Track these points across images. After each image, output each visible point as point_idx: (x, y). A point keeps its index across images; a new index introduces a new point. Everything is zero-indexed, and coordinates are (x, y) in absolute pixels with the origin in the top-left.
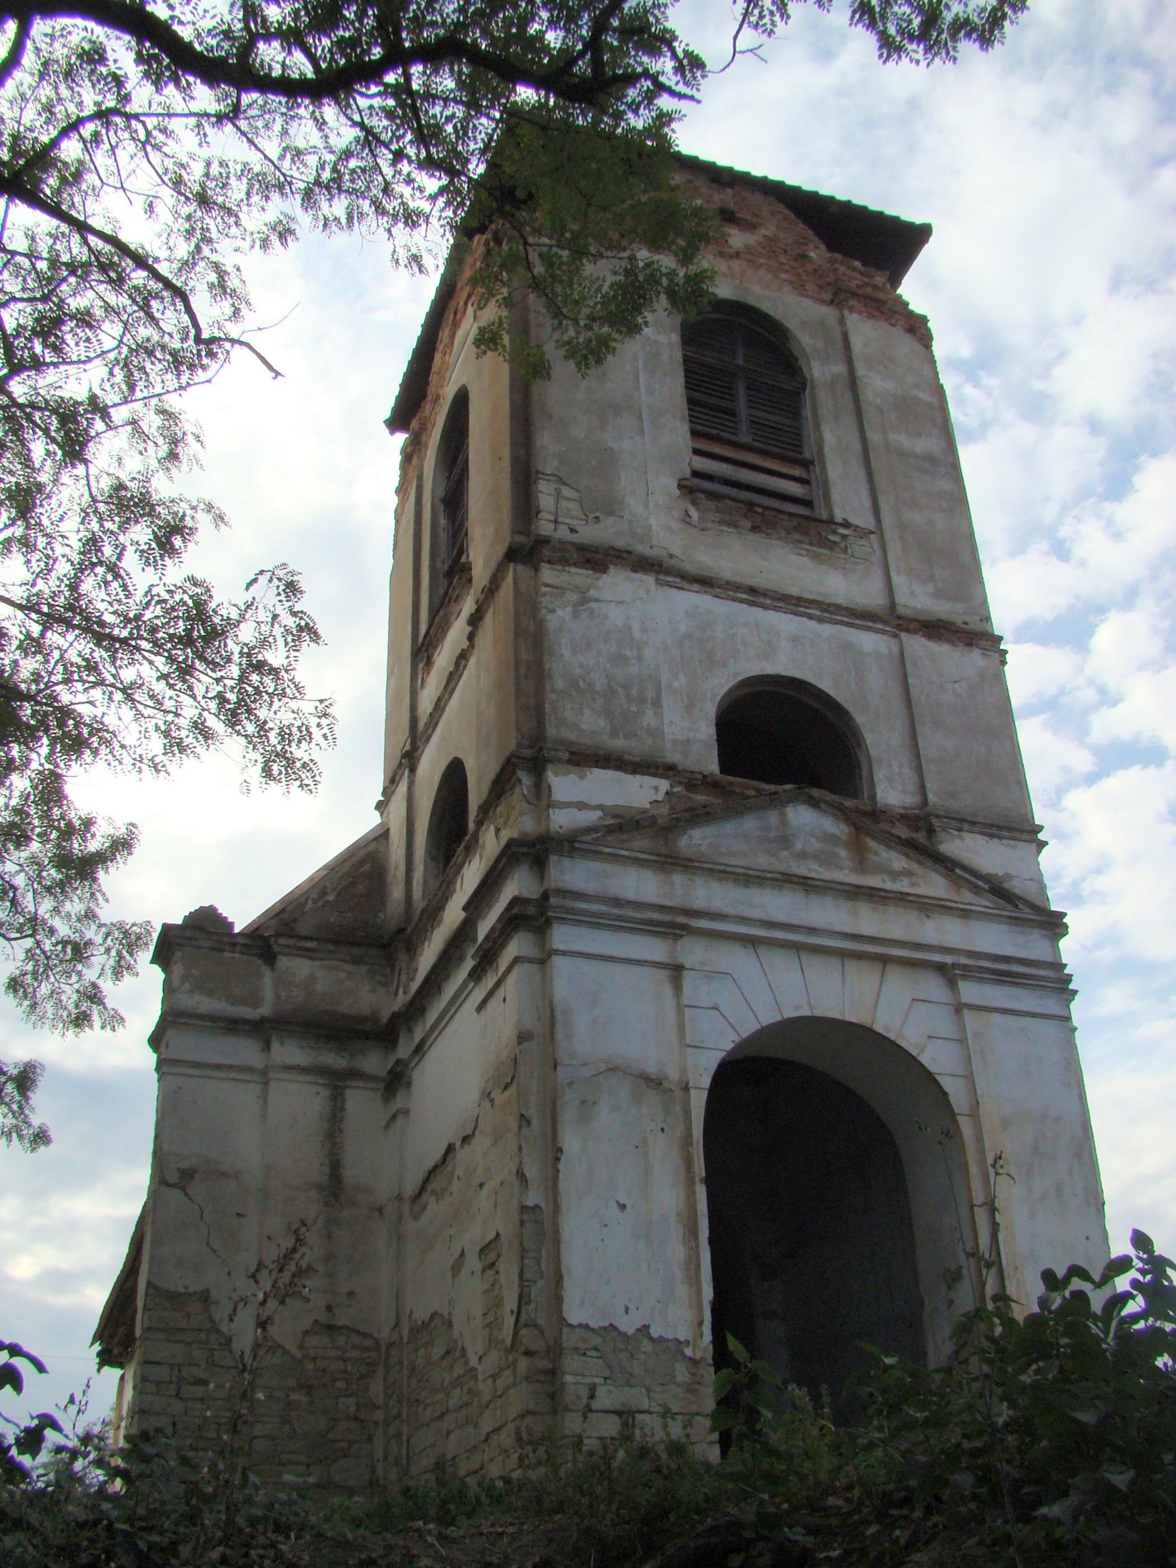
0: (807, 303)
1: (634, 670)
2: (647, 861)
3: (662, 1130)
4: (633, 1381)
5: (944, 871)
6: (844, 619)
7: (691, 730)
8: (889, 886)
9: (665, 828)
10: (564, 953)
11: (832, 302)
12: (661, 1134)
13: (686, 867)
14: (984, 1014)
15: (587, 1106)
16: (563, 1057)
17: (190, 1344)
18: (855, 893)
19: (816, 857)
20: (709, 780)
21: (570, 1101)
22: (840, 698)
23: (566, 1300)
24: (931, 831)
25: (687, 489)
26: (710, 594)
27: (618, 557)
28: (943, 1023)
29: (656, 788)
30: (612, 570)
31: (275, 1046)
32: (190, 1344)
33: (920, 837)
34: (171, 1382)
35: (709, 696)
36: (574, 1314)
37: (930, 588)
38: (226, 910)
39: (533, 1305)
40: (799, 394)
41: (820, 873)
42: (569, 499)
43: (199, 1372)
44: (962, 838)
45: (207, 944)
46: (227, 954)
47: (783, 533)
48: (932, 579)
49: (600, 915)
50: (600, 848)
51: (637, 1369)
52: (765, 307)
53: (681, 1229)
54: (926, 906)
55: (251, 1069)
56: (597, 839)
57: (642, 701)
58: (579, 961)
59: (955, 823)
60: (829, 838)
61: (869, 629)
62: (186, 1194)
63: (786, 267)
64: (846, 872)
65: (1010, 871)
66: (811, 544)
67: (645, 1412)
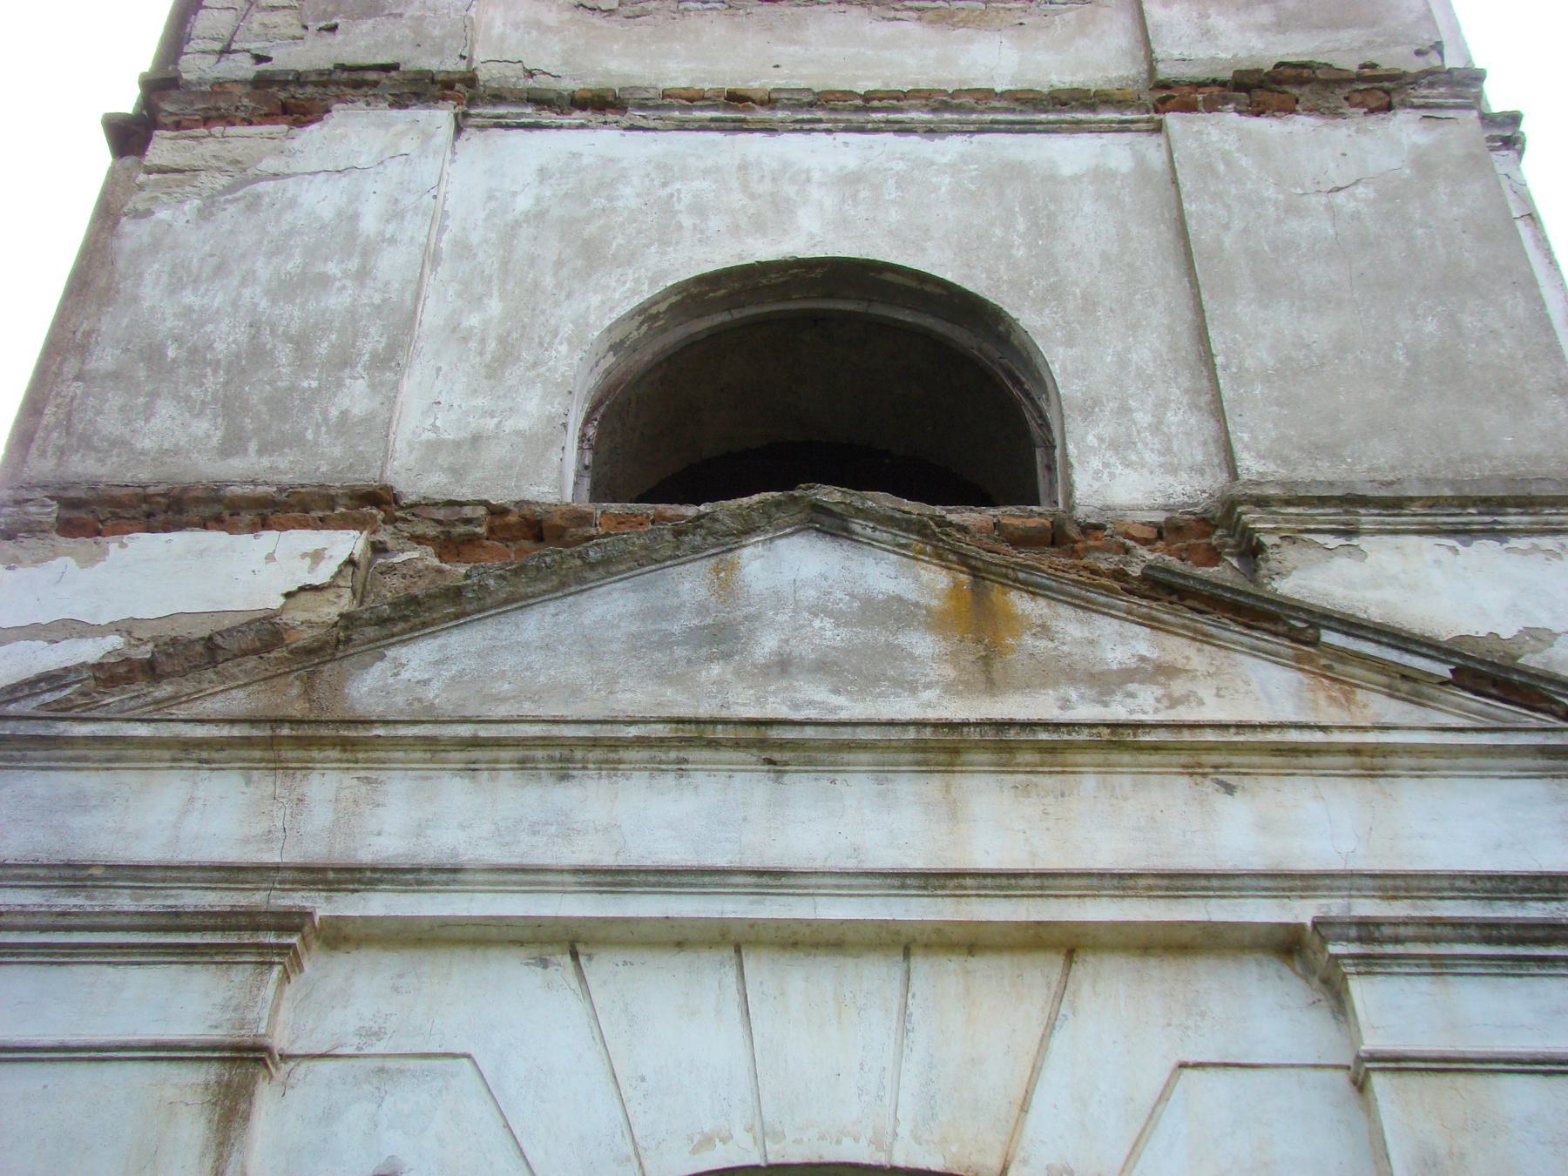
1: (337, 301)
2: (228, 743)
5: (1284, 646)
8: (1085, 712)
9: (309, 651)
13: (346, 744)
19: (824, 667)
20: (512, 519)
22: (975, 282)
24: (1252, 551)
27: (357, 85)
29: (317, 556)
33: (1225, 572)
57: (343, 360)
60: (895, 612)
64: (927, 695)
65: (1543, 620)
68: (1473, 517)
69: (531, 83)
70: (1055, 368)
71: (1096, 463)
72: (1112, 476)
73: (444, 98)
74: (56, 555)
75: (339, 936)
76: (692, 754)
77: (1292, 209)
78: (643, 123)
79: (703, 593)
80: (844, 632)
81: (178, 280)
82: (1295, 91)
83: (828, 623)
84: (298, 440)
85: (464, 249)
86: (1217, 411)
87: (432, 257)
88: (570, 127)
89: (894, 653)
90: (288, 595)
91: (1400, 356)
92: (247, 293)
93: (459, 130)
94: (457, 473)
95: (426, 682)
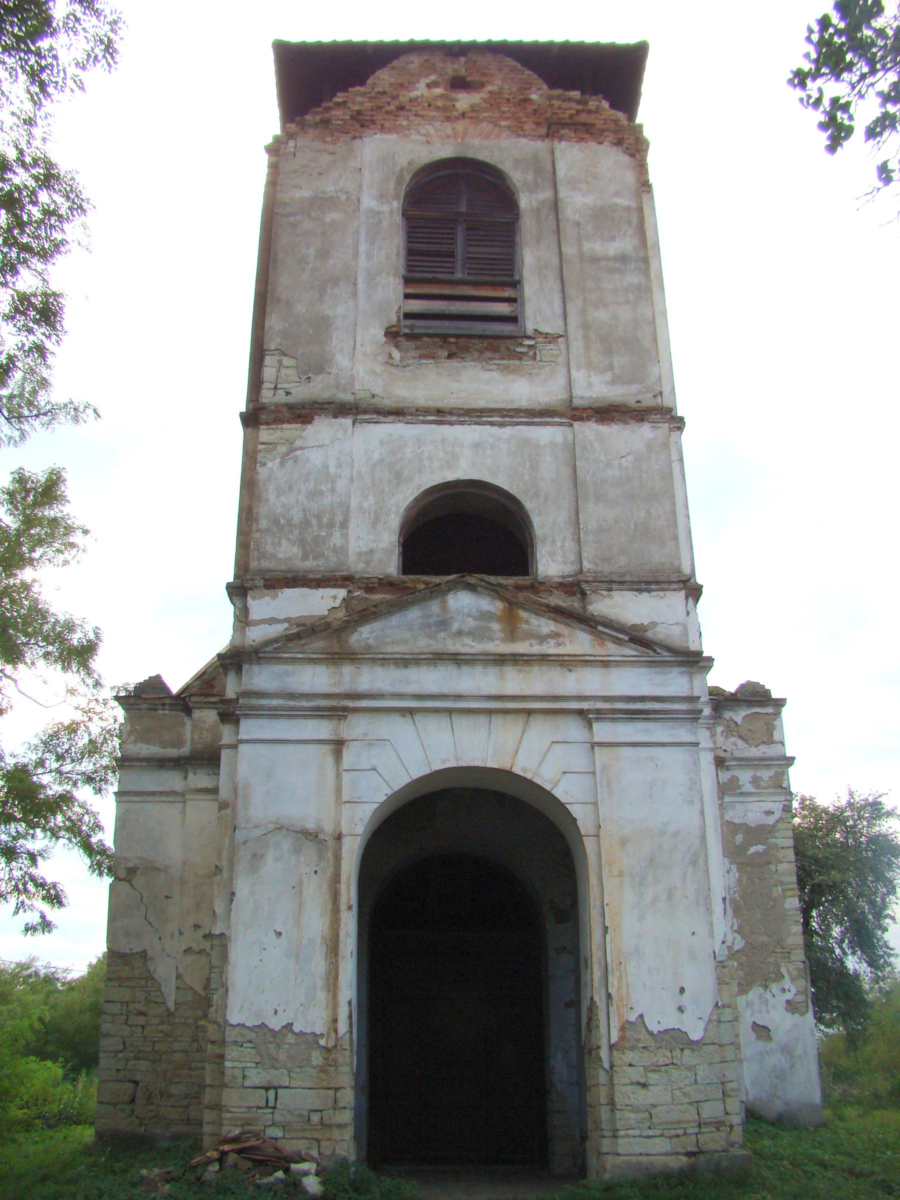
0: (523, 141)
1: (327, 500)
3: (316, 872)
4: (278, 1065)
7: (374, 541)
10: (247, 741)
11: (548, 135)
13: (352, 659)
15: (257, 857)
16: (241, 823)
17: (135, 988)
18: (500, 660)
19: (471, 634)
20: (385, 582)
21: (244, 854)
25: (392, 334)
26: (403, 422)
27: (321, 409)
28: (577, 758)
29: (335, 597)
30: (317, 420)
31: (191, 776)
32: (135, 988)
35: (393, 510)
36: (234, 1017)
37: (608, 376)
39: (214, 1007)
40: (514, 223)
42: (288, 367)
43: (141, 1007)
44: (611, 597)
45: (145, 706)
46: (160, 712)
47: (476, 355)
48: (611, 367)
49: (276, 708)
50: (280, 655)
51: (282, 1056)
52: (482, 156)
54: (568, 663)
55: (174, 793)
57: (331, 525)
58: (259, 746)
59: (604, 585)
60: (485, 616)
61: (546, 424)
62: (132, 885)
64: (497, 642)
65: (656, 619)
66: (502, 359)
68: (643, 586)
69: (373, 401)
70: (535, 525)
71: (544, 561)
73: (349, 414)
75: (355, 710)
77: (609, 465)
79: (438, 610)
80: (475, 623)
81: (279, 493)
82: (614, 414)
83: (471, 619)
84: (322, 555)
86: (579, 542)
89: (489, 629)
91: (632, 525)
92: (300, 497)
93: (354, 424)
94: (367, 563)
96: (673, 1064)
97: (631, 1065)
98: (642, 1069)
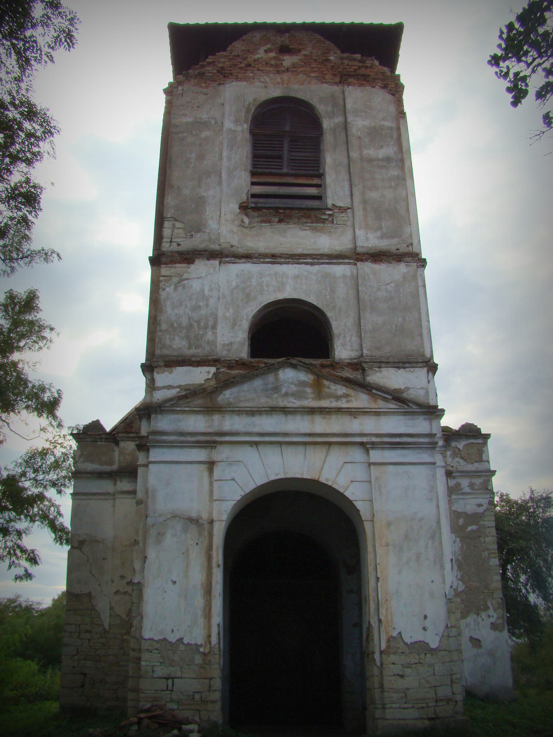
1: (203, 312)
2: (200, 411)
6: (327, 261)
7: (233, 337)
10: (154, 462)
11: (340, 82)
12: (197, 547)
14: (383, 466)
15: (161, 535)
18: (312, 411)
19: (294, 395)
21: (153, 532)
22: (320, 306)
23: (143, 628)
25: (244, 208)
27: (200, 254)
28: (359, 472)
29: (208, 372)
34: (76, 632)
35: (245, 317)
36: (147, 635)
37: (379, 234)
38: (103, 423)
41: (294, 403)
42: (179, 228)
44: (381, 372)
45: (89, 440)
46: (99, 443)
47: (296, 220)
48: (380, 228)
50: (175, 408)
52: (300, 96)
53: (202, 591)
54: (353, 413)
55: (108, 494)
56: (174, 404)
57: (206, 327)
59: (377, 364)
60: (303, 384)
61: (340, 263)
62: (82, 552)
63: (316, 69)
64: (309, 400)
65: (409, 386)
66: (312, 223)
67: (179, 678)
68: (401, 365)
69: (232, 249)
70: (333, 326)
71: (339, 349)
72: (342, 352)
74: (165, 372)
75: (222, 443)
76: (273, 412)
77: (379, 289)
78: (256, 262)
80: (296, 388)
82: (382, 257)
83: (294, 386)
85: (224, 297)
86: (360, 337)
87: (219, 299)
88: (241, 263)
90: (205, 380)
91: (394, 327)
92: (186, 310)
94: (229, 351)
95: (229, 398)
96: (420, 663)
97: (393, 664)
98: (400, 666)
